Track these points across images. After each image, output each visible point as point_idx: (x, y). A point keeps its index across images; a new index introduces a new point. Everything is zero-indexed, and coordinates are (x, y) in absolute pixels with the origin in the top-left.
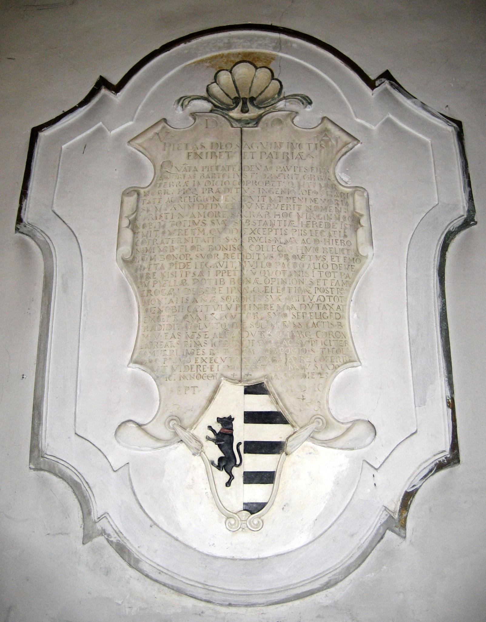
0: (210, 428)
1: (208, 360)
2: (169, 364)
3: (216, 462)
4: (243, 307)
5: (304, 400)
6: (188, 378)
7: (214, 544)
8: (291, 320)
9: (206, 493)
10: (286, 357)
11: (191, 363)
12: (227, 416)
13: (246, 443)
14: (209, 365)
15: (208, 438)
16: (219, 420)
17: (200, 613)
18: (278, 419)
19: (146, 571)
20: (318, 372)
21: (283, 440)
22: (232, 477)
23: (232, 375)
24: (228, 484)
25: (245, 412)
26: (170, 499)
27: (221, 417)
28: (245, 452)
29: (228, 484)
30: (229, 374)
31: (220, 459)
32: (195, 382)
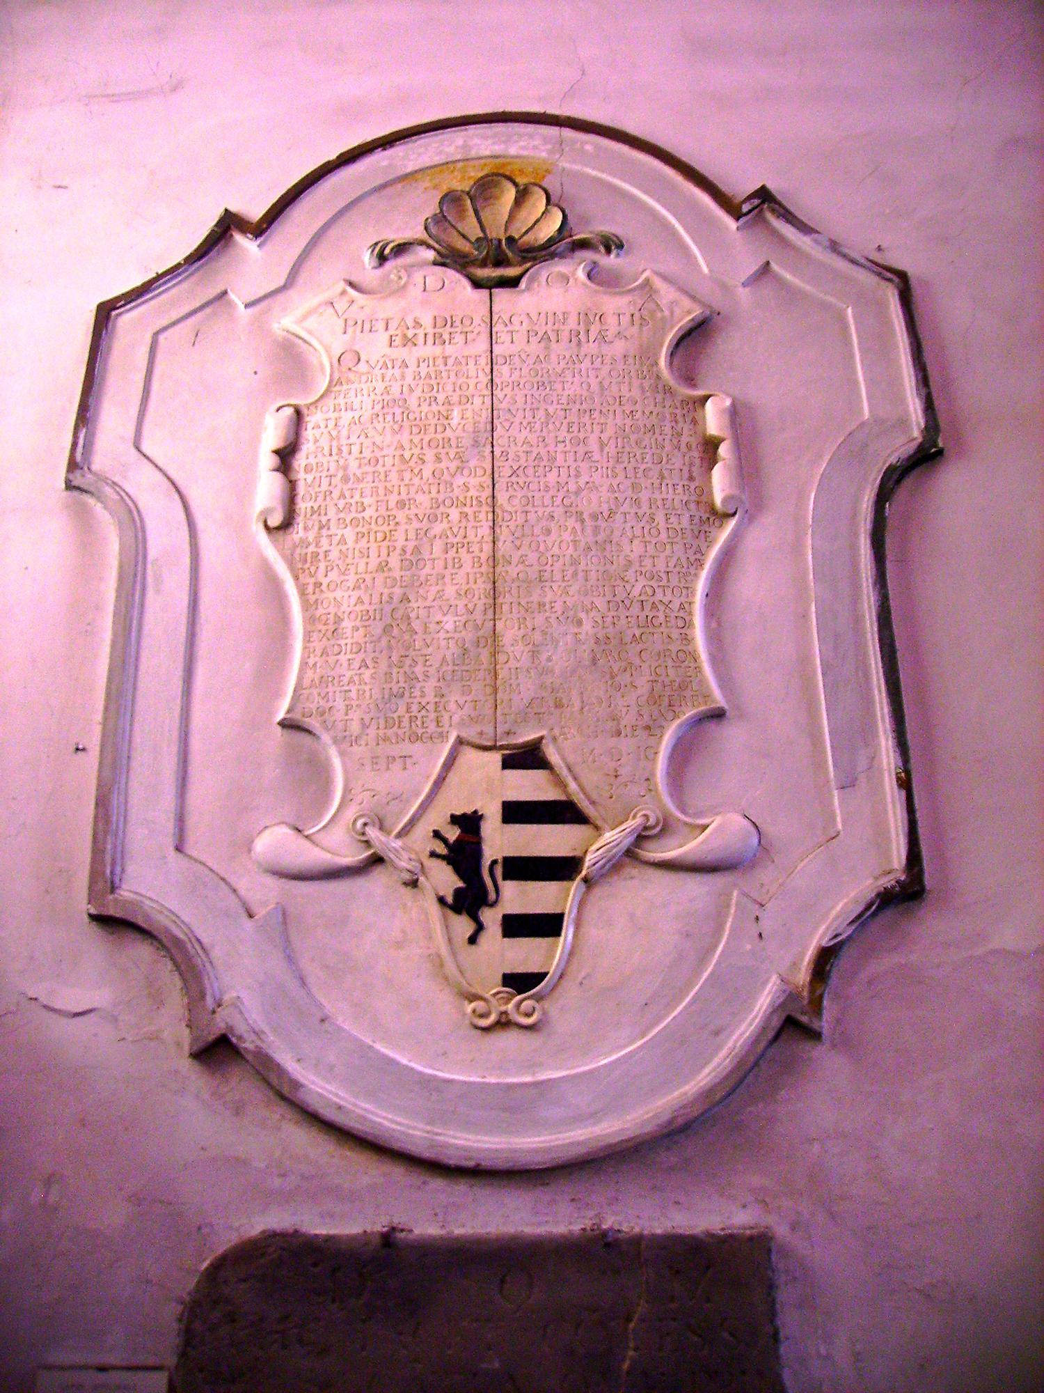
0: (437, 834)
1: (431, 707)
3: (450, 900)
8: (591, 631)
12: (469, 810)
13: (508, 862)
15: (433, 854)
16: (455, 820)
21: (578, 853)
22: (480, 927)
24: (473, 940)
25: (504, 803)
28: (505, 878)
29: (473, 940)
30: (470, 734)
31: (458, 892)
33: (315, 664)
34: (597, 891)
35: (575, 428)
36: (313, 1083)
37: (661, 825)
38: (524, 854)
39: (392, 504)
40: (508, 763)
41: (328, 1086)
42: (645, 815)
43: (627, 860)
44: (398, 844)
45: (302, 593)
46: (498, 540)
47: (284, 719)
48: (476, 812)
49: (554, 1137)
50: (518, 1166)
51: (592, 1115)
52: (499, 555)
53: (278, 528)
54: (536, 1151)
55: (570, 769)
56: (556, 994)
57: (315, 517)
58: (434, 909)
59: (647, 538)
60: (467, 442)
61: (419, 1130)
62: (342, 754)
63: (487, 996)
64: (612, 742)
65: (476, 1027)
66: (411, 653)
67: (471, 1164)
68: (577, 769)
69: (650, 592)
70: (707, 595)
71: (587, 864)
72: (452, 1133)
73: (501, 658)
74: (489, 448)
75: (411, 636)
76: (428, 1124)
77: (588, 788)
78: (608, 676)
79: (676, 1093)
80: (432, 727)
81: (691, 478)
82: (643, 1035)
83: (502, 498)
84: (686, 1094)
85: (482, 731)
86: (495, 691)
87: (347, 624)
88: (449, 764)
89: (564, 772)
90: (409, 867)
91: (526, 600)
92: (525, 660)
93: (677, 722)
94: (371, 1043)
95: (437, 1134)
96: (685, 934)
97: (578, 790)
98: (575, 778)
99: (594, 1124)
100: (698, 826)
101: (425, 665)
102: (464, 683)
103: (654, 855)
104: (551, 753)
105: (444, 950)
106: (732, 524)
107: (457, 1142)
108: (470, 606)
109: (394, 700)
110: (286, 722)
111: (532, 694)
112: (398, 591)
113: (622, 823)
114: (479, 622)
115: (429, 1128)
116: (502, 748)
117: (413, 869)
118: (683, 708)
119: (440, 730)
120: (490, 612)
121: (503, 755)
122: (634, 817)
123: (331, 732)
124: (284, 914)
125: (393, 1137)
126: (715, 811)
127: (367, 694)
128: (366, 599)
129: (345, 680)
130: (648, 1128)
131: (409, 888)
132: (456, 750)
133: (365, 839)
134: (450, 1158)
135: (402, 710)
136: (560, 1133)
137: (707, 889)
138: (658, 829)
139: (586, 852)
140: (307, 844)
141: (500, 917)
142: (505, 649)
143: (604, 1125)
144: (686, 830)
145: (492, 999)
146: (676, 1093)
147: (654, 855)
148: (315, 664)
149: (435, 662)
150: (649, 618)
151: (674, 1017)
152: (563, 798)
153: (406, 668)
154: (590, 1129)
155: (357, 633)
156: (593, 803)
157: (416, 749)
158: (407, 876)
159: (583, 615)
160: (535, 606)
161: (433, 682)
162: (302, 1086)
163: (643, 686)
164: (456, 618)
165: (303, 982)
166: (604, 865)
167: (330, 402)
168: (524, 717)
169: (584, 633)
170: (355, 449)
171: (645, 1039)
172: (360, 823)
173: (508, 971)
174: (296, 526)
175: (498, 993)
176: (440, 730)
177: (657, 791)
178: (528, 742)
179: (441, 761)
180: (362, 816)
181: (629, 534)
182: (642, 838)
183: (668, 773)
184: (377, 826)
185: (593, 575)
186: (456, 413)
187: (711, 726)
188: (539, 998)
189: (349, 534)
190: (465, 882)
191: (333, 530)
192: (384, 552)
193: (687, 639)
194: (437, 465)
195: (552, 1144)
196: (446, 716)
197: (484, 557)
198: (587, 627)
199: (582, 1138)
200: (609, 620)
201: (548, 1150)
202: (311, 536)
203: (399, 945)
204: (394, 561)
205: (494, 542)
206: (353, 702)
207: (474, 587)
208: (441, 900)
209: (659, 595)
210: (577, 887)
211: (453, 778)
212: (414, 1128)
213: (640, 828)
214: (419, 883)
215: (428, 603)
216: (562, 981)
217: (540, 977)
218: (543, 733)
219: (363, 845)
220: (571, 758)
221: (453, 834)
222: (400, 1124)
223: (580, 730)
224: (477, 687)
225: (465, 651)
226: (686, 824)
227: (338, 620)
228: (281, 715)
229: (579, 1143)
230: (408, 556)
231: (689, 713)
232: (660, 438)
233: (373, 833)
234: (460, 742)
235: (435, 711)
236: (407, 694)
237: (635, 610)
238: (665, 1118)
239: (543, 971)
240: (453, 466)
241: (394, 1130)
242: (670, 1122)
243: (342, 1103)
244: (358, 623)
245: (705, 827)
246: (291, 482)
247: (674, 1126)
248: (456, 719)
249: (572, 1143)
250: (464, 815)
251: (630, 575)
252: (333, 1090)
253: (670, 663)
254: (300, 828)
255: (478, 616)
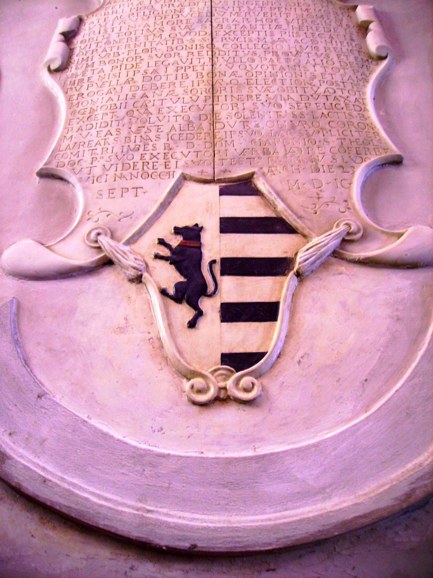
0: (162, 242)
1: (161, 156)
2: (99, 164)
3: (171, 291)
4: (216, 99)
5: (320, 199)
6: (128, 177)
7: (162, 429)
8: (289, 111)
9: (149, 340)
10: (285, 148)
11: (134, 161)
12: (190, 223)
13: (224, 261)
14: (162, 161)
15: (157, 257)
16: (177, 231)
17: (128, 570)
18: (278, 227)
19: (17, 478)
20: (339, 165)
21: (289, 255)
22: (200, 314)
23: (199, 172)
24: (192, 324)
25: (221, 218)
26: (82, 352)
27: (181, 225)
28: (223, 274)
29: (192, 324)
30: (194, 172)
31: (178, 286)
32: (139, 182)
33: (72, 137)
34: (309, 285)
35: (269, 15)
36: (22, 456)
37: (362, 231)
38: (240, 256)
39: (139, 50)
40: (223, 192)
41: (36, 460)
42: (346, 224)
43: (334, 260)
44: (127, 248)
45: (69, 100)
46: (216, 64)
47: (42, 169)
48: (196, 225)
49: (278, 514)
50: (239, 547)
51: (322, 490)
52: (216, 71)
53: (57, 70)
54: (260, 530)
55: (278, 194)
56: (275, 371)
57: (84, 62)
58: (155, 298)
59: (325, 64)
60: (194, 20)
61: (129, 506)
62: (84, 188)
63: (207, 373)
64: (314, 175)
65: (195, 403)
66: (147, 124)
67: (186, 545)
68: (284, 195)
69: (331, 91)
70: (374, 99)
71: (298, 260)
72: (165, 510)
73: (218, 126)
74: (209, 23)
75: (148, 116)
76: (140, 501)
77: (294, 206)
78: (305, 136)
79: (410, 466)
80: (161, 168)
81: (352, 40)
82: (367, 408)
83: (218, 44)
84: (420, 465)
85: (202, 170)
86: (214, 145)
87: (100, 112)
88: (174, 192)
89: (273, 197)
90: (135, 265)
91: (237, 94)
92: (238, 127)
93: (364, 164)
94: (86, 419)
95: (149, 511)
96: (396, 318)
97: (286, 208)
98: (283, 200)
99: (324, 499)
100: (393, 234)
101: (158, 131)
102: (188, 141)
103: (358, 254)
104: (261, 184)
105: (163, 333)
106: (385, 63)
107: (170, 520)
108: (194, 98)
109: (130, 152)
110: (43, 172)
111: (243, 146)
112: (140, 93)
113: (327, 231)
114: (201, 107)
115: (140, 505)
116: (219, 181)
117: (138, 267)
118: (369, 156)
119: (167, 170)
120: (210, 101)
121: (220, 186)
122: (338, 226)
123: (78, 176)
124: (19, 307)
125: (98, 513)
126: (406, 225)
127: (110, 151)
128: (115, 98)
129: (93, 144)
130: (386, 502)
131: (134, 284)
132: (181, 183)
133: (96, 245)
134: (161, 539)
135: (137, 157)
136: (286, 510)
137: (409, 282)
138: (360, 235)
139: (296, 254)
140: (47, 251)
141: (219, 305)
142: (221, 121)
143: (336, 500)
144: (384, 237)
145: (210, 375)
146: (410, 466)
147: (358, 254)
148: (72, 137)
149: (166, 129)
150: (333, 105)
151: (397, 391)
152: (273, 215)
153: (143, 134)
154: (319, 506)
155: (133, 258)
156: (300, 217)
157: (147, 183)
158: (132, 273)
159: (282, 103)
160: (245, 97)
161: (164, 140)
162: (9, 458)
163: (334, 141)
164: (183, 105)
165: (26, 362)
166: (315, 261)
167: (103, 12)
168: (237, 161)
169: (283, 112)
170: (116, 30)
171: (369, 413)
172: (93, 235)
173: (226, 351)
174: (70, 69)
175: (218, 369)
176: (167, 170)
177: (354, 209)
178: (241, 176)
179: (168, 190)
180: (96, 229)
181: (313, 62)
182: (346, 242)
183: (362, 201)
184: (109, 235)
185: (288, 82)
186: (187, 10)
187: (392, 170)
188: (258, 375)
189: (107, 68)
190: (185, 277)
191: (96, 66)
192: (131, 74)
193: (365, 117)
194: (172, 32)
195: (278, 522)
196: (173, 162)
197: (205, 73)
198: (286, 107)
199: (311, 515)
200: (303, 105)
201: (275, 528)
202: (79, 72)
203: (121, 330)
204: (138, 78)
205: (213, 66)
206: (97, 156)
207: (198, 88)
208: (163, 292)
209: (339, 93)
210: (291, 279)
211: (177, 202)
212: (125, 505)
213: (345, 233)
214: (143, 279)
215: (162, 97)
216: (280, 360)
217: (257, 357)
218: (255, 170)
219: (95, 250)
220: (279, 187)
221: (175, 241)
222: (106, 499)
223: (285, 167)
224: (199, 144)
225: (189, 123)
226: (383, 232)
227: (92, 110)
228: (40, 165)
229: (309, 520)
230: (149, 74)
231: (373, 158)
232: (328, 21)
233: (105, 241)
234: (184, 178)
235: (164, 159)
236: (142, 149)
237: (322, 100)
238: (400, 493)
239: (261, 350)
240: (183, 32)
241: (101, 506)
242: (408, 495)
243: (49, 477)
244: (108, 111)
245: (400, 235)
246: (70, 49)
247: (412, 500)
248: (181, 163)
249: (301, 521)
250: (186, 228)
251: (316, 82)
252: (41, 463)
253: (353, 129)
254: (44, 243)
255: (201, 103)
